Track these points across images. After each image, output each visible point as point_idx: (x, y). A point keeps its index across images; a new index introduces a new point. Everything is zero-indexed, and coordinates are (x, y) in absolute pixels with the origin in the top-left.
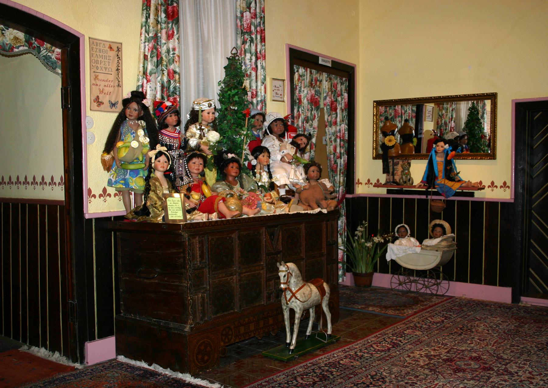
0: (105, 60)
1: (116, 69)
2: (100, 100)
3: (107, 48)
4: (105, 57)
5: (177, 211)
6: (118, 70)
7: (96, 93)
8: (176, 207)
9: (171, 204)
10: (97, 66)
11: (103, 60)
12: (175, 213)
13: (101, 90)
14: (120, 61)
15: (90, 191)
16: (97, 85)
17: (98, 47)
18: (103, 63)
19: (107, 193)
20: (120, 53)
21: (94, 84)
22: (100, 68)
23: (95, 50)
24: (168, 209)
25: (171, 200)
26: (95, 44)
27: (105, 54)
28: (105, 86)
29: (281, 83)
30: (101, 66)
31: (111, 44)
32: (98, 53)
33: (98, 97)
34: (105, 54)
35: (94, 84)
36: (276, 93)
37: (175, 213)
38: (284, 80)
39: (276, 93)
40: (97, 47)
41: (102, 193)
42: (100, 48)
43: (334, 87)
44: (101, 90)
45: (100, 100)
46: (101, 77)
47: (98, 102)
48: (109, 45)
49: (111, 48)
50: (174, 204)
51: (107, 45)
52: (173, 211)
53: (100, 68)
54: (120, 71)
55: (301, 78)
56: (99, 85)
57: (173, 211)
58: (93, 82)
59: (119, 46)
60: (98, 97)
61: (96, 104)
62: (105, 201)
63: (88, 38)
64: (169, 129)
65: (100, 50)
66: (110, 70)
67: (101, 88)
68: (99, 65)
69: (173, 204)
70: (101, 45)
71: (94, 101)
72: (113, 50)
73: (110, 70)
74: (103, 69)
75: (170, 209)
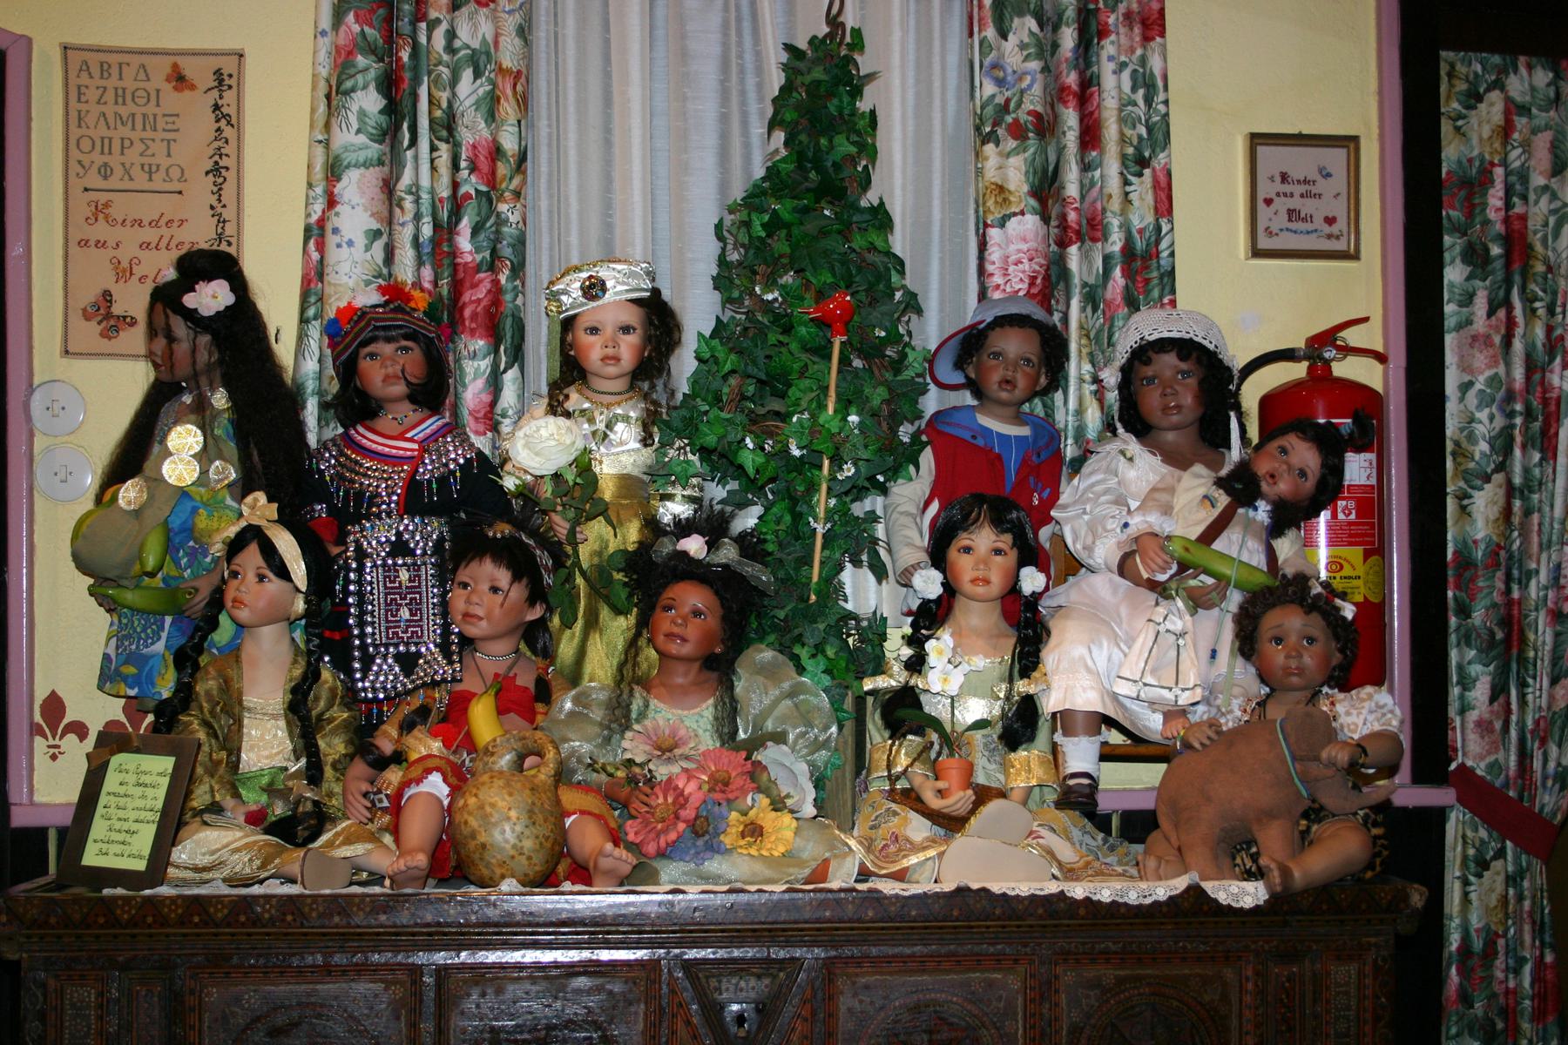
0: (149, 134)
1: (209, 165)
2: (117, 310)
3: (159, 80)
4: (150, 123)
5: (135, 827)
6: (216, 170)
7: (96, 276)
8: (140, 803)
9: (122, 790)
10: (106, 165)
11: (135, 136)
12: (120, 837)
13: (125, 264)
14: (228, 132)
15: (54, 706)
16: (101, 244)
17: (113, 82)
18: (139, 147)
19: (65, 721)
20: (229, 96)
21: (83, 243)
22: (119, 171)
23: (92, 95)
24: (100, 810)
25: (132, 767)
26: (96, 71)
27: (151, 109)
28: (145, 246)
29: (1336, 158)
30: (127, 159)
31: (180, 60)
32: (110, 110)
33: (107, 296)
34: (151, 109)
35: (83, 243)
36: (1290, 212)
37: (120, 837)
38: (1349, 143)
39: (1290, 212)
40: (103, 83)
41: (123, 719)
42: (120, 84)
43: (473, 169)
44: (125, 264)
45: (117, 310)
46: (122, 206)
47: (108, 316)
48: (168, 70)
49: (179, 80)
50: (139, 791)
51: (162, 67)
52: (118, 825)
53: (119, 171)
54: (231, 176)
55: (1521, 122)
56: (111, 243)
57: (118, 825)
58: (81, 231)
59: (229, 66)
60: (107, 296)
61: (94, 328)
62: (54, 757)
63: (56, 56)
64: (385, 422)
65: (120, 96)
66: (175, 173)
67: (125, 255)
68: (115, 161)
69: (131, 790)
70: (128, 73)
71: (87, 316)
72: (193, 87)
73: (175, 173)
74: (136, 172)
75: (112, 811)
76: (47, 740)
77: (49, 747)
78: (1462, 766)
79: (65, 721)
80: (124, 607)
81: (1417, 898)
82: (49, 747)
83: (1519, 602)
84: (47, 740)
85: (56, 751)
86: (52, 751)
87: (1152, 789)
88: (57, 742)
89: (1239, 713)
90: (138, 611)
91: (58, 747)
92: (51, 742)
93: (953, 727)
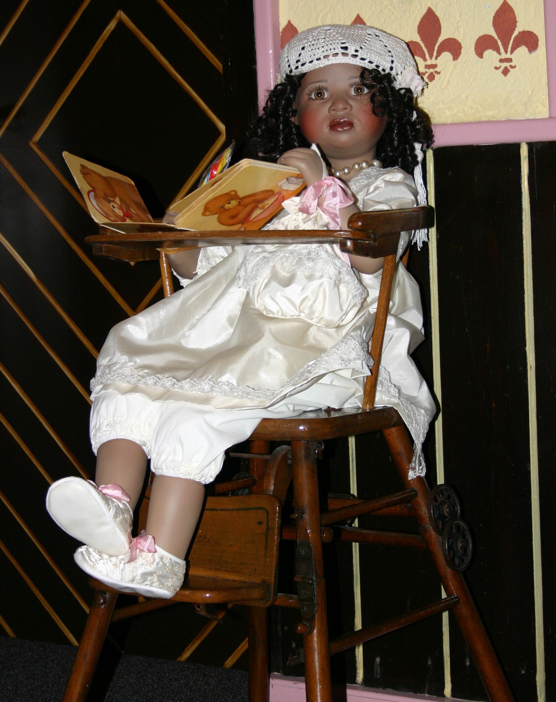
19: (441, 39)
62: (506, 72)
76: (499, 53)
77: (501, 61)
78: (159, 252)
79: (441, 39)
80: (421, 408)
81: (278, 156)
82: (501, 61)
83: (427, 125)
84: (499, 53)
85: (507, 64)
86: (504, 65)
87: (392, 208)
88: (508, 56)
89: (307, 69)
90: (336, 345)
91: (510, 60)
92: (504, 56)
93: (287, 157)
